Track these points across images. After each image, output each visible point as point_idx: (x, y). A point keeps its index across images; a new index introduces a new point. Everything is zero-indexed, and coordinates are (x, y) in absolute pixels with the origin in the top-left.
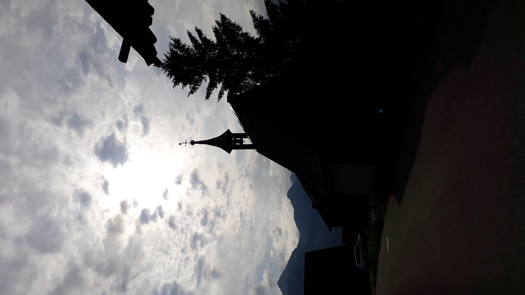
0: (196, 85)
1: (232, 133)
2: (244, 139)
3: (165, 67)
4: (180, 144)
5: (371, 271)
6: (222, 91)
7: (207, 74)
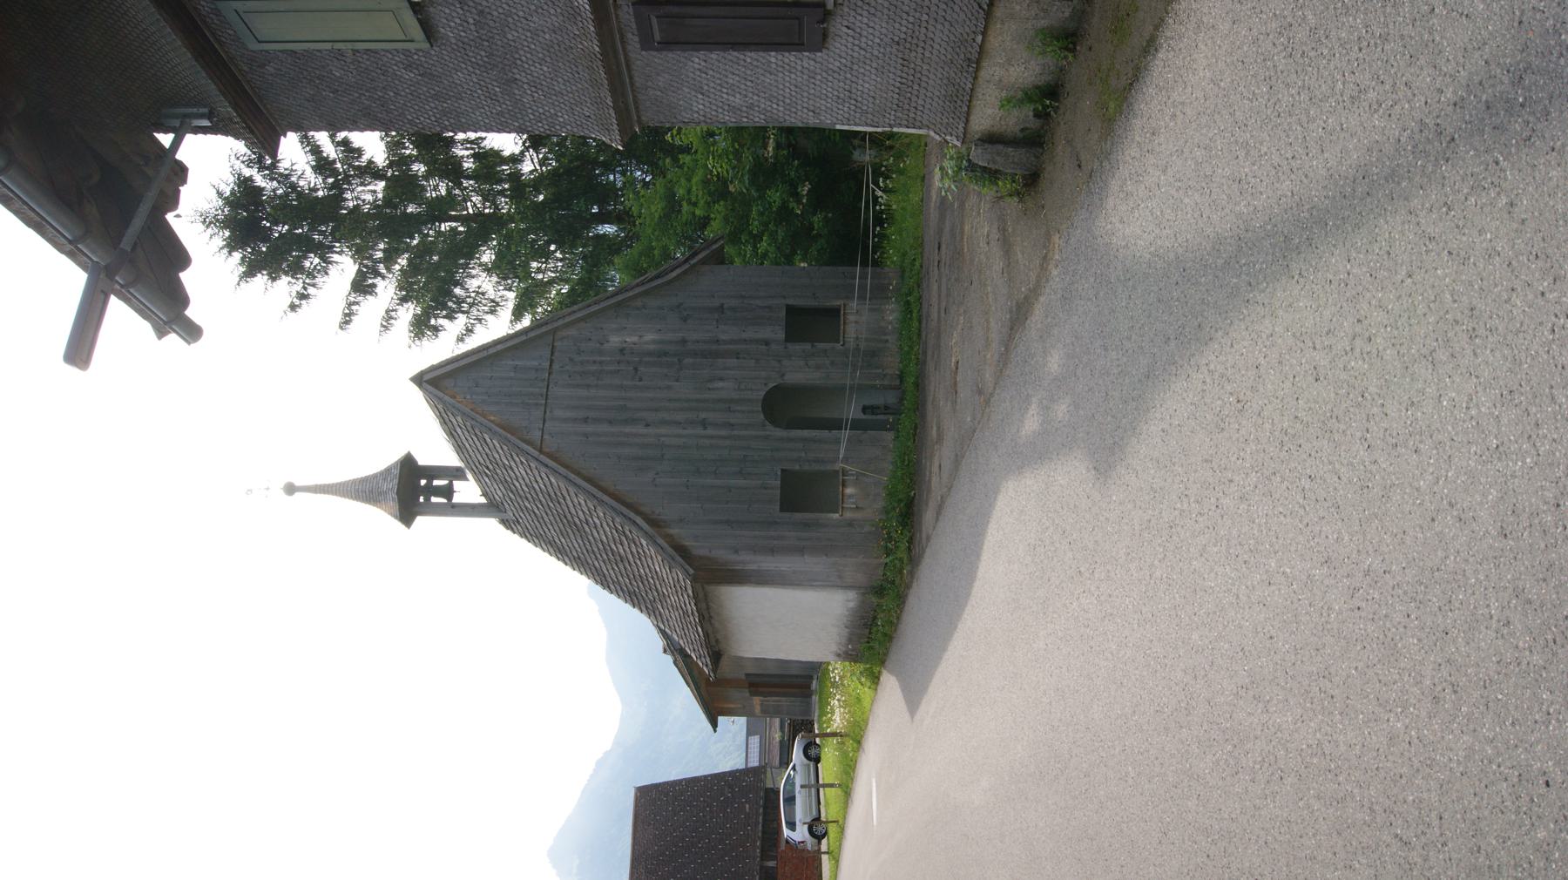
0: (309, 284)
1: (421, 463)
2: (457, 484)
3: (211, 223)
4: (249, 490)
5: (824, 853)
6: (393, 311)
7: (345, 212)
